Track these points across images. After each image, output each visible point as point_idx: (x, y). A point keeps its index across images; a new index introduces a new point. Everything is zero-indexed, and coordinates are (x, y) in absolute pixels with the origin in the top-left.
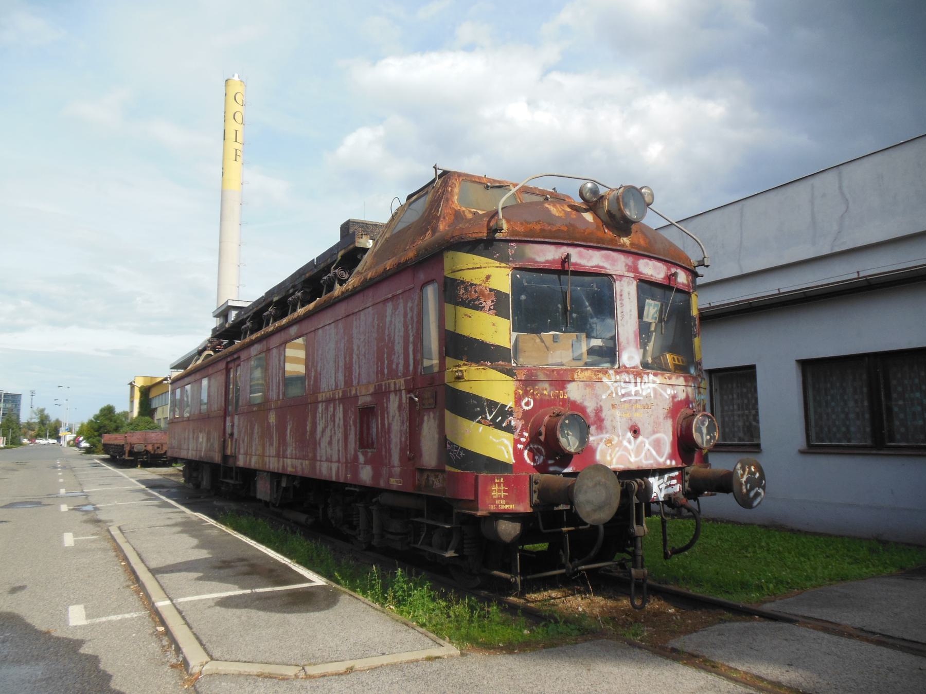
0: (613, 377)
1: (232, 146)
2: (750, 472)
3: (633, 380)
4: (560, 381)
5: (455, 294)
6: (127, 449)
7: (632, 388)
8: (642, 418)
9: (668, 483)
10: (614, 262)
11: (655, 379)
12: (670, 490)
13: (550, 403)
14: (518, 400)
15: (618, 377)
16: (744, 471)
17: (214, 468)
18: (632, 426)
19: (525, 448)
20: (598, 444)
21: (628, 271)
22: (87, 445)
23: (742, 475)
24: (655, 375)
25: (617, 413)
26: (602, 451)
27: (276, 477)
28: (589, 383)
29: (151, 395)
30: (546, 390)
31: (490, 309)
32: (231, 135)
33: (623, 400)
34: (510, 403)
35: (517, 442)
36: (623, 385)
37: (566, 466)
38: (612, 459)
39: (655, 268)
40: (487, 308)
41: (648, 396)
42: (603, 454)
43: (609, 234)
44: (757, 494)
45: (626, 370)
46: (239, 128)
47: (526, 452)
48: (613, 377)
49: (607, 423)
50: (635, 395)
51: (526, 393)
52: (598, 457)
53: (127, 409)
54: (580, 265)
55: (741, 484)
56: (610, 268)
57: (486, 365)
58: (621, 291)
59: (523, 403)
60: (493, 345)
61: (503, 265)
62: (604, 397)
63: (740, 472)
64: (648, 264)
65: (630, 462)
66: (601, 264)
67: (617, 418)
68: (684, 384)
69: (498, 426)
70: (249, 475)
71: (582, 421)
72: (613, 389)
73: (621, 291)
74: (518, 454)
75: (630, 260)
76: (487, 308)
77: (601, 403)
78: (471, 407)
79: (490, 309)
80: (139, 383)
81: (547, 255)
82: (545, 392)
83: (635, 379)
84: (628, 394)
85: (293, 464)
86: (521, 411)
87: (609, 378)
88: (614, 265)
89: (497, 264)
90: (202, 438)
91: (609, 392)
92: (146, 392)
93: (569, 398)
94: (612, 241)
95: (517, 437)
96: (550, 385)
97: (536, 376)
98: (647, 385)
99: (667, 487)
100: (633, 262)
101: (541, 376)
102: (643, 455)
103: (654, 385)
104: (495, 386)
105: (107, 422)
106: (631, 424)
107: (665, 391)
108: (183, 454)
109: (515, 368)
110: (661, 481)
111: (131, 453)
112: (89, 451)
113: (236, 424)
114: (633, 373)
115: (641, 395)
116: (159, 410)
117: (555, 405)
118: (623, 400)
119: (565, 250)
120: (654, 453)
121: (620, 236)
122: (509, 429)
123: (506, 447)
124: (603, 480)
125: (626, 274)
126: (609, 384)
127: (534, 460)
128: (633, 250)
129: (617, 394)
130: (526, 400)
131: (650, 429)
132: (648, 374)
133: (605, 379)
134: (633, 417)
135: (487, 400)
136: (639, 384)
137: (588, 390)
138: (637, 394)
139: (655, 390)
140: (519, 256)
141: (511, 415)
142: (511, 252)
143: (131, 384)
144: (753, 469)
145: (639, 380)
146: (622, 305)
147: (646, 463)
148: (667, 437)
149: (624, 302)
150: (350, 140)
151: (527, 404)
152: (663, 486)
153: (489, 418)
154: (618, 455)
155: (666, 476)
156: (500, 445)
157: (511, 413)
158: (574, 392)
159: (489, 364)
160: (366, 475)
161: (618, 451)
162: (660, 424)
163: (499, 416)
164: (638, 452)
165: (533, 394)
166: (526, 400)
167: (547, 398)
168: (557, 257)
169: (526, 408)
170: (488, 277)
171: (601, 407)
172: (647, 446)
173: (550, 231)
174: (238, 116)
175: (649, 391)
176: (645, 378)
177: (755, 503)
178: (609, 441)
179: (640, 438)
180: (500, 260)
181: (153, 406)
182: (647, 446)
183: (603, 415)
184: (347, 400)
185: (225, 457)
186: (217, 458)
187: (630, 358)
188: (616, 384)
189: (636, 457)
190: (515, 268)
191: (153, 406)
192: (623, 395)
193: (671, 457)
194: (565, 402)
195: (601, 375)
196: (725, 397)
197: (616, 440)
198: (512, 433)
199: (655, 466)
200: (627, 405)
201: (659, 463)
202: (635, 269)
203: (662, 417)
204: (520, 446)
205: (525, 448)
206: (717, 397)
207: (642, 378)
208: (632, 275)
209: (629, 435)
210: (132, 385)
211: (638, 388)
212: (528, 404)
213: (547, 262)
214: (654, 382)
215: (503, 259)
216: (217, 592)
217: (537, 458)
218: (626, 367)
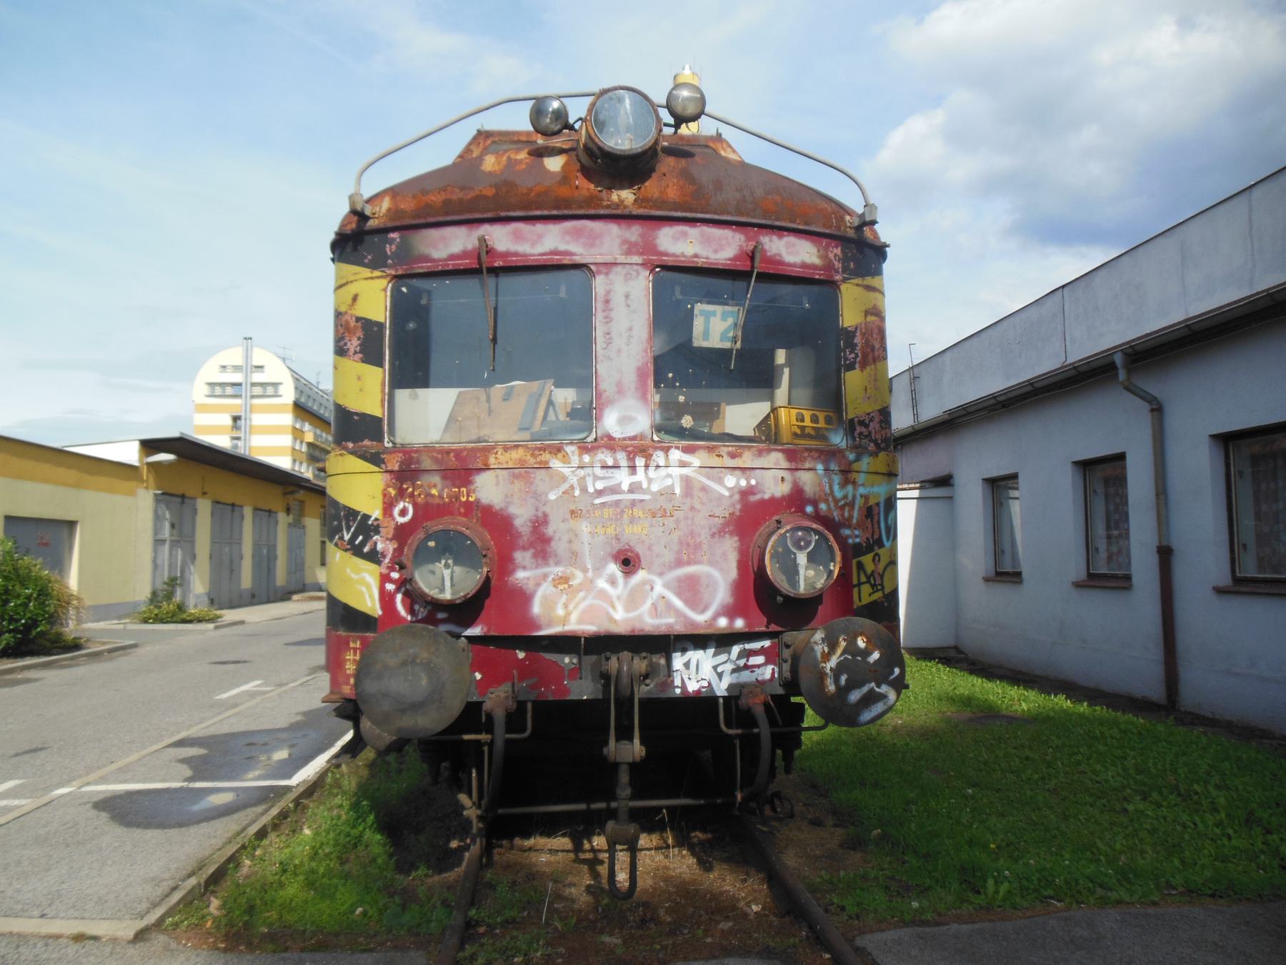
0: (575, 460)
2: (851, 649)
3: (623, 462)
7: (623, 478)
8: (637, 534)
9: (742, 662)
10: (593, 239)
11: (687, 458)
12: (746, 677)
13: (442, 510)
14: (388, 507)
15: (587, 458)
16: (833, 646)
18: (619, 552)
19: (398, 590)
20: (538, 585)
21: (628, 253)
23: (827, 657)
24: (687, 450)
25: (584, 527)
26: (545, 598)
28: (521, 472)
30: (435, 487)
31: (356, 352)
33: (597, 501)
34: (376, 513)
35: (385, 579)
36: (599, 472)
37: (470, 624)
38: (568, 614)
39: (706, 241)
40: (352, 351)
41: (667, 493)
42: (549, 604)
43: (585, 186)
44: (871, 698)
45: (610, 443)
47: (399, 597)
48: (575, 460)
49: (559, 546)
50: (631, 491)
51: (401, 494)
52: (537, 608)
54: (516, 254)
55: (822, 675)
56: (579, 251)
57: (346, 448)
58: (608, 292)
59: (396, 511)
60: (357, 414)
61: (377, 273)
62: (552, 496)
63: (820, 648)
64: (685, 234)
65: (611, 619)
66: (562, 247)
67: (585, 537)
68: (785, 464)
69: (357, 551)
71: (497, 540)
72: (574, 480)
73: (608, 292)
74: (387, 600)
75: (634, 232)
76: (352, 351)
77: (547, 509)
79: (356, 352)
81: (452, 243)
82: (434, 492)
83: (631, 459)
84: (615, 490)
86: (392, 525)
87: (566, 459)
88: (592, 245)
89: (366, 272)
91: (565, 486)
93: (477, 501)
94: (592, 200)
95: (385, 571)
96: (444, 478)
97: (418, 462)
98: (663, 472)
99: (737, 670)
100: (642, 236)
101: (427, 463)
102: (648, 604)
103: (685, 471)
106: (617, 547)
107: (720, 481)
109: (386, 451)
110: (723, 657)
114: (624, 448)
115: (648, 491)
117: (451, 513)
118: (597, 501)
119: (485, 229)
120: (678, 603)
121: (610, 189)
122: (374, 557)
123: (368, 586)
124: (424, 655)
125: (622, 259)
126: (567, 471)
127: (411, 611)
128: (641, 211)
129: (584, 490)
130: (401, 505)
131: (669, 556)
132: (666, 450)
133: (556, 463)
135: (345, 507)
136: (640, 471)
137: (518, 485)
138: (634, 488)
139: (687, 481)
140: (405, 254)
141: (377, 532)
142: (389, 249)
144: (861, 643)
145: (640, 462)
146: (608, 320)
147: (649, 620)
148: (719, 576)
149: (613, 314)
150: (897, 137)
151: (403, 512)
152: (729, 667)
153: (347, 537)
154: (582, 606)
155: (736, 649)
157: (376, 529)
158: (488, 489)
159: (350, 445)
161: (576, 597)
162: (698, 546)
164: (633, 600)
165: (412, 495)
166: (401, 505)
167: (437, 501)
168: (470, 246)
169: (401, 520)
170: (355, 298)
171: (545, 515)
172: (659, 588)
173: (461, 201)
175: (669, 482)
176: (659, 457)
177: (867, 716)
178: (564, 579)
179: (641, 575)
180: (373, 266)
182: (659, 588)
183: (550, 531)
187: (623, 421)
188: (582, 472)
189: (627, 610)
190: (395, 277)
192: (600, 493)
193: (731, 612)
194: (470, 507)
195: (546, 456)
196: (1263, 486)
197: (578, 578)
198: (379, 563)
199: (680, 629)
200: (608, 512)
201: (693, 624)
202: (648, 248)
203: (704, 536)
204: (390, 587)
205: (398, 590)
206: (1245, 490)
207: (649, 458)
208: (637, 259)
209: (614, 568)
211: (640, 476)
212: (404, 513)
213: (452, 257)
214: (683, 465)
215: (377, 263)
216: (139, 782)
217: (417, 607)
218: (610, 438)
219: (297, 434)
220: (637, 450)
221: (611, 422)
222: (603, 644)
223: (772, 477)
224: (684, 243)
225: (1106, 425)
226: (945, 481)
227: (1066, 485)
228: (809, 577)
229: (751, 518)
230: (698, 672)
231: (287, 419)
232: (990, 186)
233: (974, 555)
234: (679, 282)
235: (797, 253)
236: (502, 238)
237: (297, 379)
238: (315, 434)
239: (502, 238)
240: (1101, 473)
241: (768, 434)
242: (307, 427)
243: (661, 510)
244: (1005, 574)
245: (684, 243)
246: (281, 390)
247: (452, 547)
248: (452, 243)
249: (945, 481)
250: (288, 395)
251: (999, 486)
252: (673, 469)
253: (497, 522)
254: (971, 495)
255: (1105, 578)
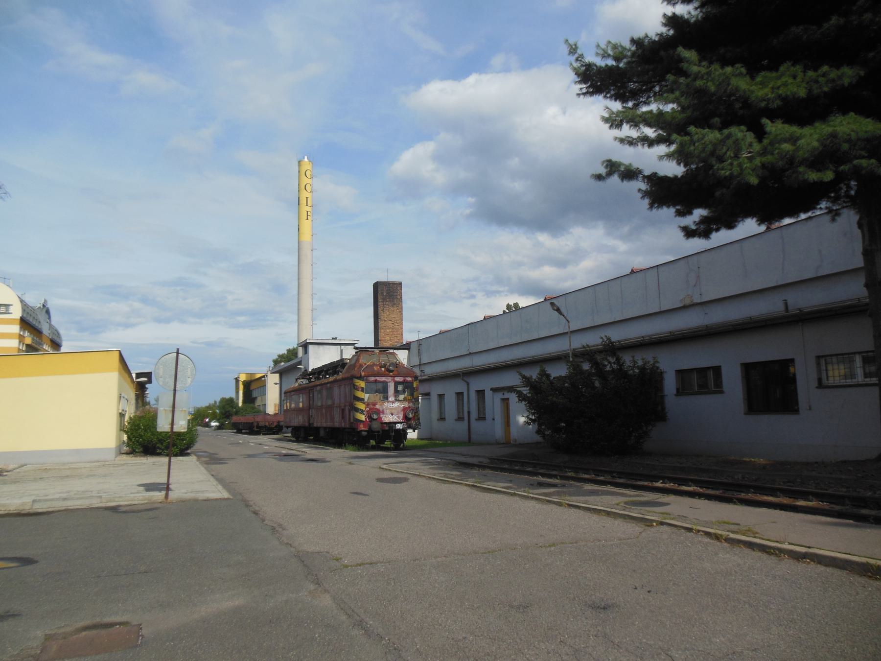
1: (305, 209)
4: (375, 405)
5: (356, 388)
6: (255, 424)
8: (393, 411)
17: (305, 428)
22: (217, 424)
27: (325, 428)
29: (253, 387)
32: (303, 201)
46: (309, 195)
53: (233, 396)
70: (317, 429)
71: (378, 412)
78: (357, 410)
80: (243, 378)
81: (372, 379)
85: (329, 424)
90: (300, 417)
92: (247, 385)
104: (362, 406)
105: (230, 409)
108: (292, 424)
111: (258, 427)
112: (219, 428)
113: (313, 412)
116: (259, 399)
134: (392, 411)
143: (236, 379)
148: (401, 416)
156: (362, 417)
158: (377, 406)
160: (343, 425)
161: (388, 418)
163: (362, 412)
174: (308, 187)
181: (254, 396)
184: (340, 407)
185: (310, 424)
186: (307, 424)
191: (254, 396)
210: (237, 380)
219: (21, 338)
220: (393, 402)
221: (390, 399)
222: (390, 423)
223: (406, 405)
224: (398, 379)
225: (459, 386)
226: (428, 394)
227: (454, 397)
228: (411, 416)
229: (404, 409)
230: (399, 426)
231: (16, 329)
232: (456, 189)
233: (435, 415)
234: (397, 384)
235: (409, 379)
236: (378, 378)
237: (25, 306)
238: (33, 339)
239: (378, 378)
240: (459, 395)
241: (405, 399)
242: (27, 334)
243: (395, 408)
244: (442, 419)
245: (398, 379)
246: (11, 309)
247: (375, 413)
248: (372, 379)
249: (428, 394)
250: (16, 312)
251: (441, 397)
252: (397, 404)
253: (378, 410)
254: (434, 398)
255: (460, 419)
